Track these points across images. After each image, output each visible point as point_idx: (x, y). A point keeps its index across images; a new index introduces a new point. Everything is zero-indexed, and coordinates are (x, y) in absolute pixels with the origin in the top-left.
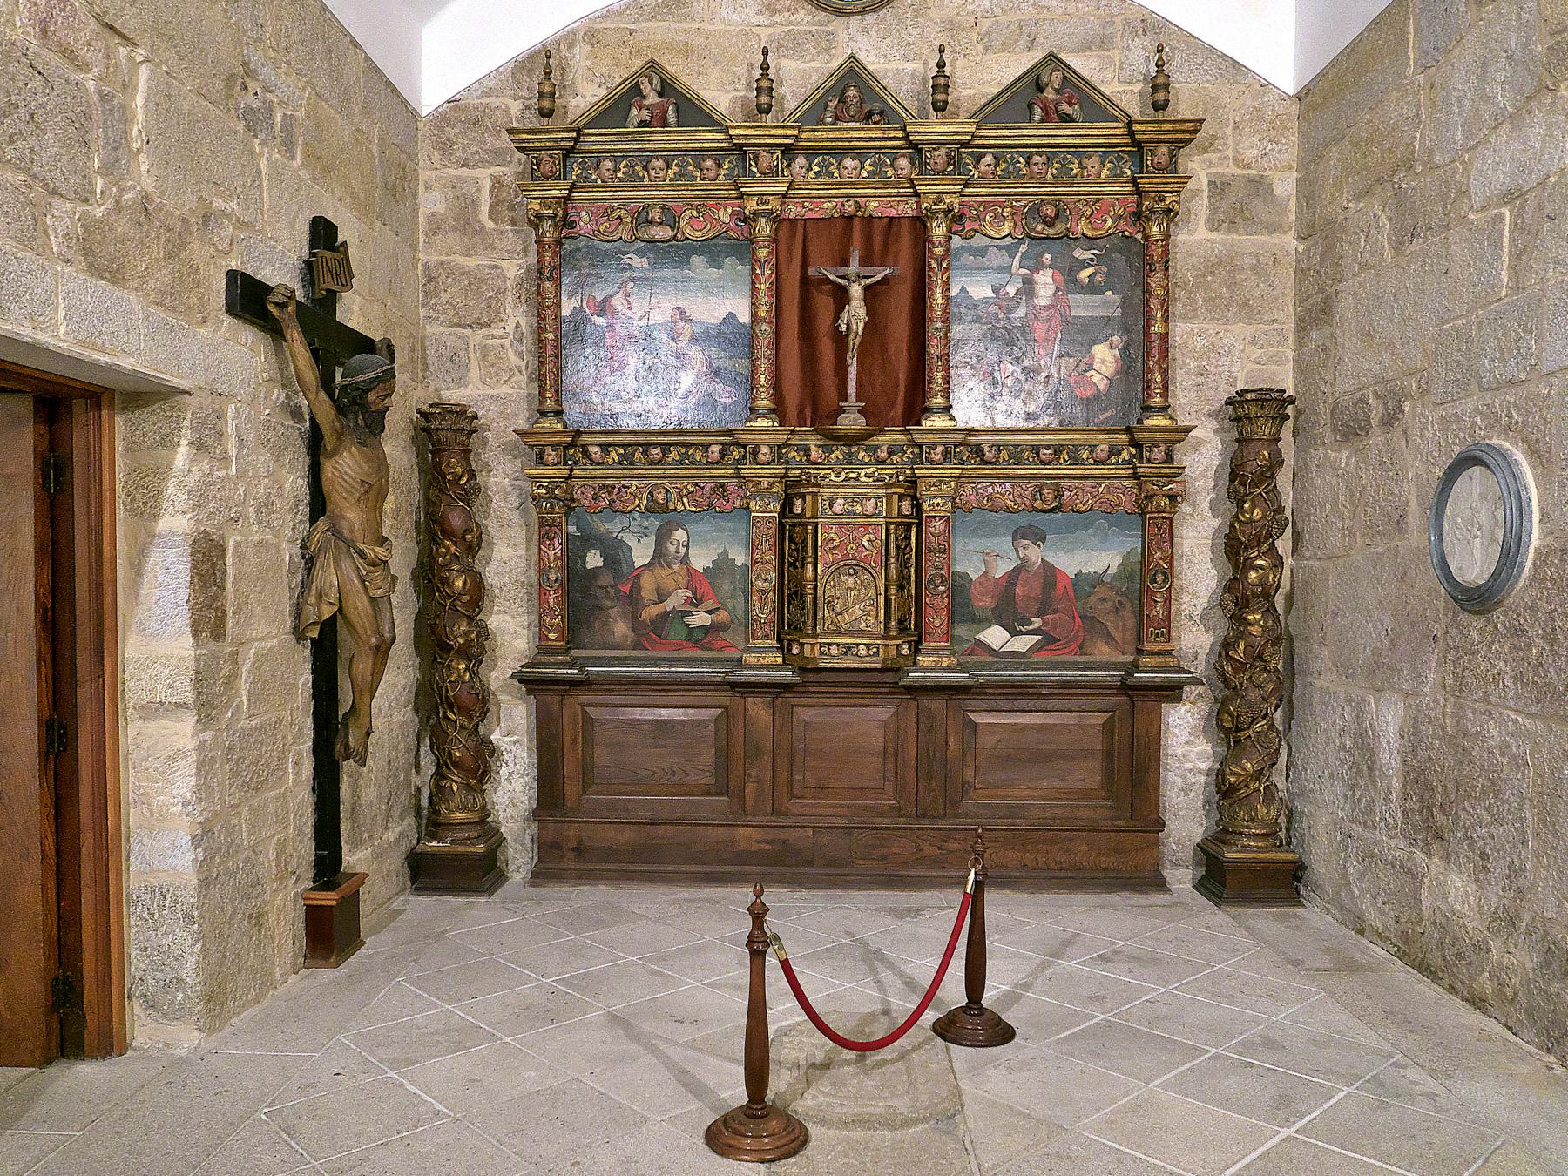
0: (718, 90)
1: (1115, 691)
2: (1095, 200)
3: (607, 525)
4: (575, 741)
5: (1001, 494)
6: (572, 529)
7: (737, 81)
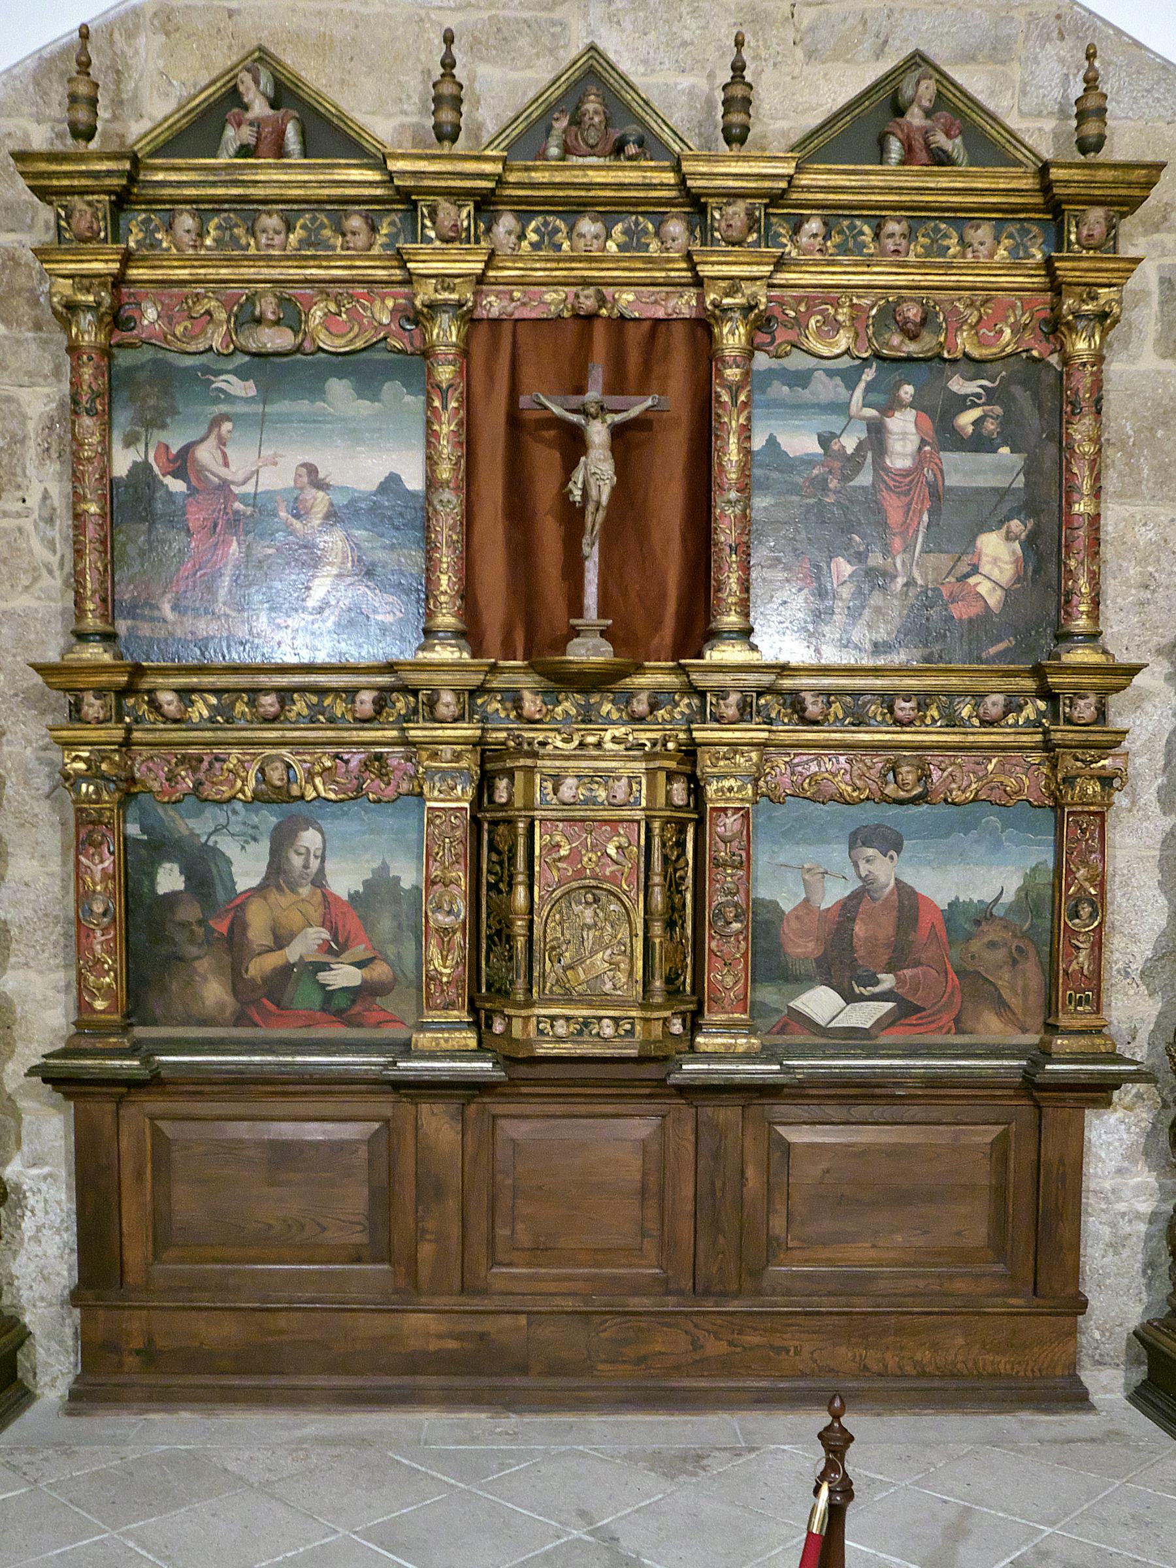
0: (373, 113)
1: (1011, 1092)
2: (984, 296)
3: (193, 823)
4: (139, 1176)
5: (831, 773)
6: (133, 830)
7: (404, 97)
